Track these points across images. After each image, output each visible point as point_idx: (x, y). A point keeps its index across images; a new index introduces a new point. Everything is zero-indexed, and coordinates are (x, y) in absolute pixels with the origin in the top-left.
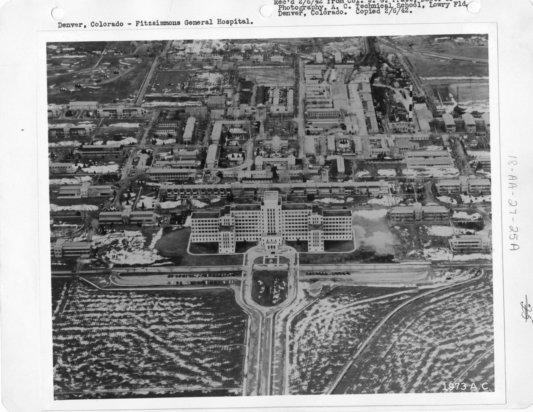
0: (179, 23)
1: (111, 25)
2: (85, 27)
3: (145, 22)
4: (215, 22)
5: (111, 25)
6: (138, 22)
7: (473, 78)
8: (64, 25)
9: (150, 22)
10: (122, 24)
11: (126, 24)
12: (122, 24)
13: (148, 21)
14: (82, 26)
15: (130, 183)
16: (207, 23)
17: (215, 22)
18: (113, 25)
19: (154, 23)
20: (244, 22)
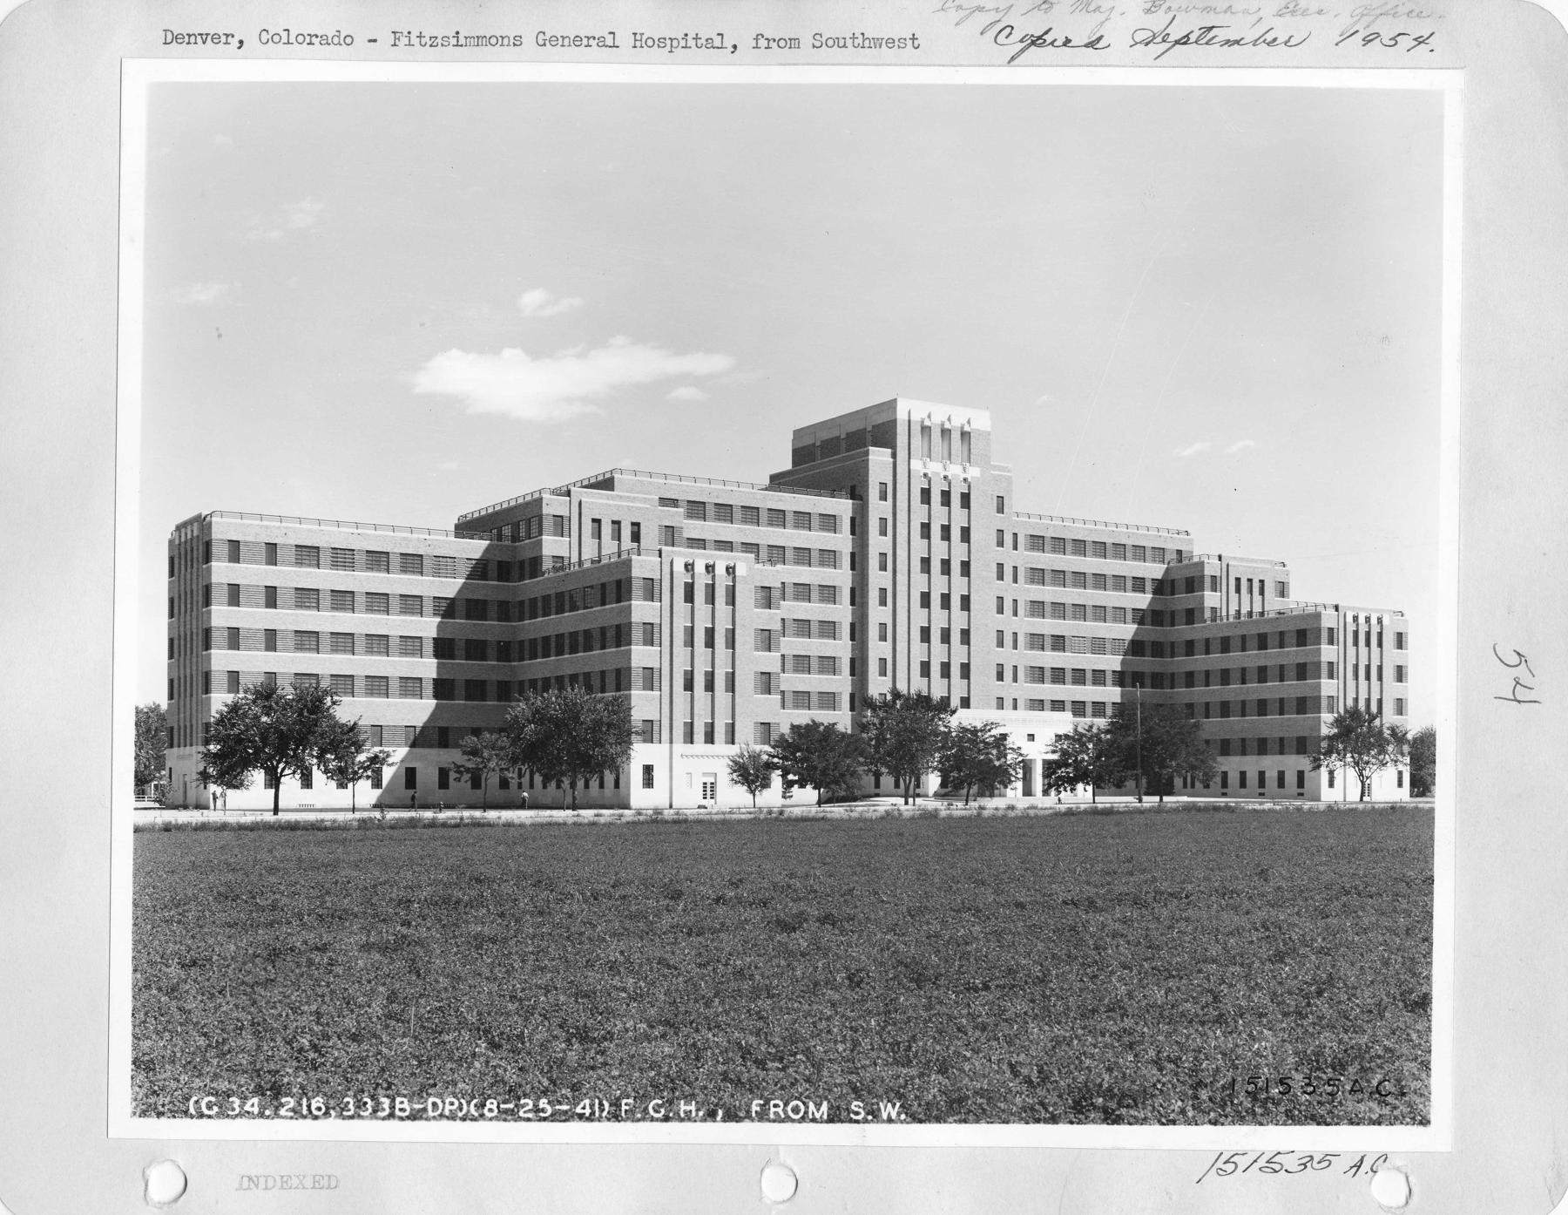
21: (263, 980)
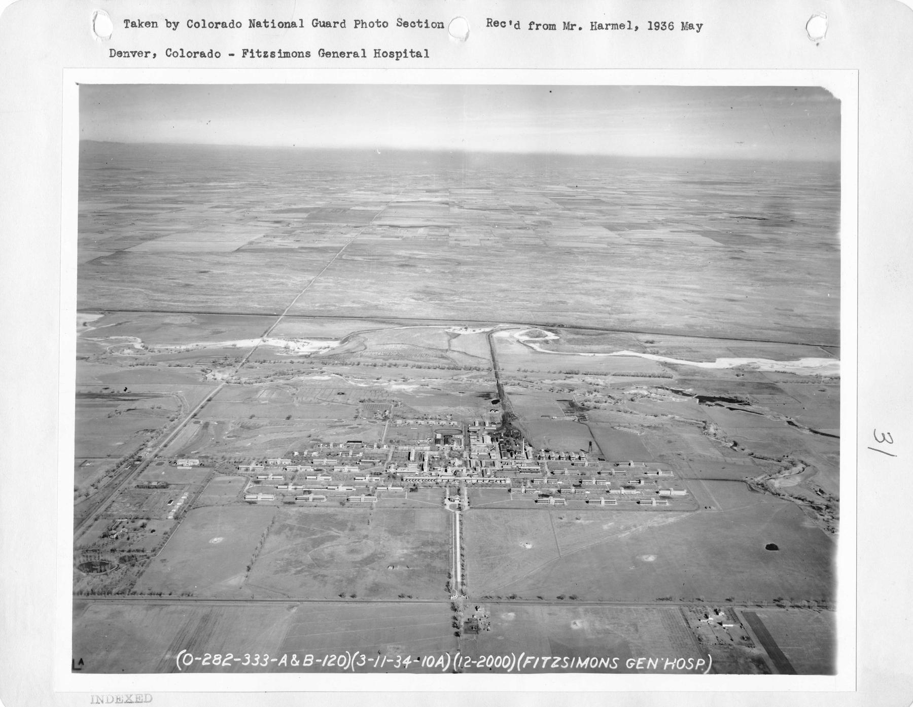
0: (308, 54)
1: (198, 55)
2: (580, 29)
3: (258, 52)
4: (370, 53)
5: (198, 55)
6: (245, 52)
7: (356, 258)
8: (120, 54)
9: (266, 53)
10: (218, 55)
11: (225, 55)
12: (218, 55)
13: (262, 50)
14: (150, 56)
15: (326, 558)
16: (356, 55)
17: (370, 53)
18: (203, 55)
19: (273, 53)
20: (419, 55)
21: (128, 582)
